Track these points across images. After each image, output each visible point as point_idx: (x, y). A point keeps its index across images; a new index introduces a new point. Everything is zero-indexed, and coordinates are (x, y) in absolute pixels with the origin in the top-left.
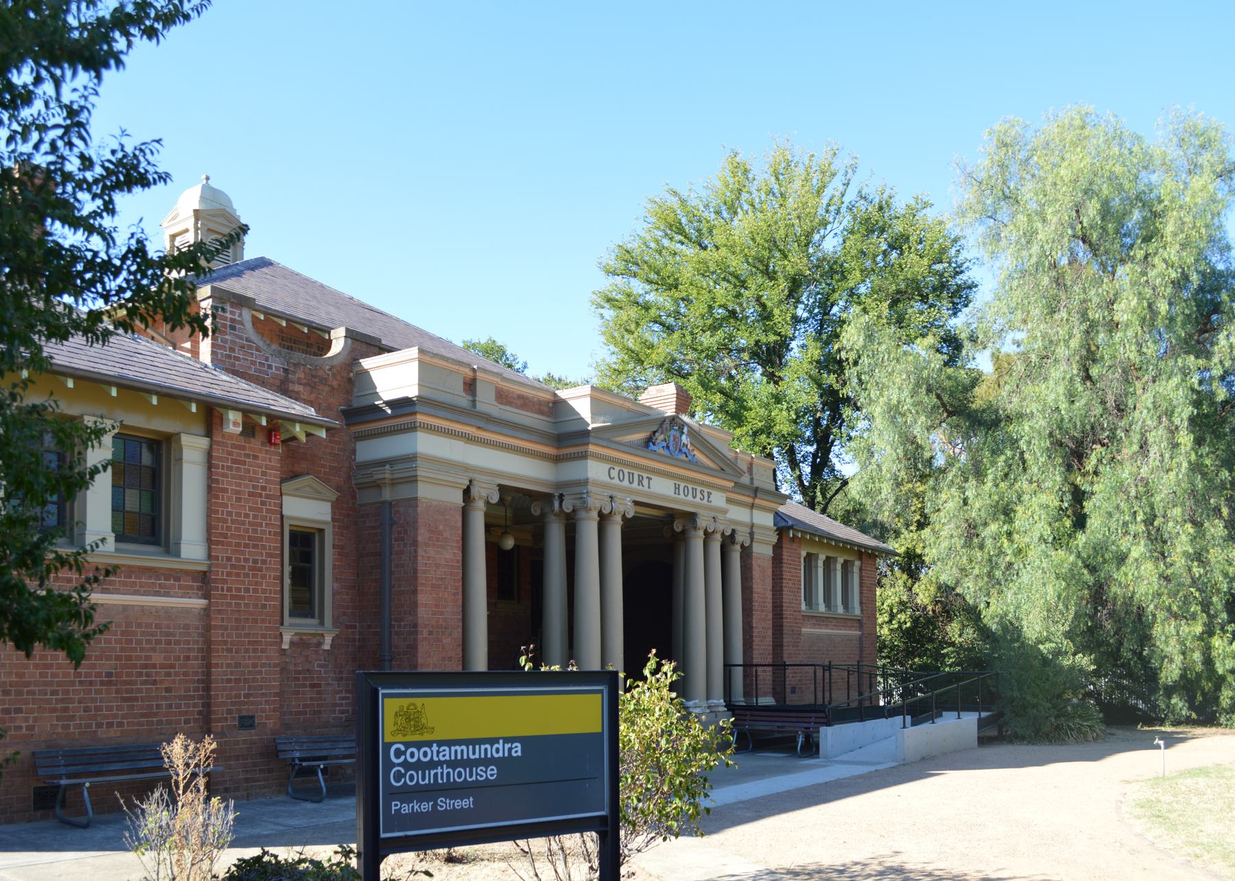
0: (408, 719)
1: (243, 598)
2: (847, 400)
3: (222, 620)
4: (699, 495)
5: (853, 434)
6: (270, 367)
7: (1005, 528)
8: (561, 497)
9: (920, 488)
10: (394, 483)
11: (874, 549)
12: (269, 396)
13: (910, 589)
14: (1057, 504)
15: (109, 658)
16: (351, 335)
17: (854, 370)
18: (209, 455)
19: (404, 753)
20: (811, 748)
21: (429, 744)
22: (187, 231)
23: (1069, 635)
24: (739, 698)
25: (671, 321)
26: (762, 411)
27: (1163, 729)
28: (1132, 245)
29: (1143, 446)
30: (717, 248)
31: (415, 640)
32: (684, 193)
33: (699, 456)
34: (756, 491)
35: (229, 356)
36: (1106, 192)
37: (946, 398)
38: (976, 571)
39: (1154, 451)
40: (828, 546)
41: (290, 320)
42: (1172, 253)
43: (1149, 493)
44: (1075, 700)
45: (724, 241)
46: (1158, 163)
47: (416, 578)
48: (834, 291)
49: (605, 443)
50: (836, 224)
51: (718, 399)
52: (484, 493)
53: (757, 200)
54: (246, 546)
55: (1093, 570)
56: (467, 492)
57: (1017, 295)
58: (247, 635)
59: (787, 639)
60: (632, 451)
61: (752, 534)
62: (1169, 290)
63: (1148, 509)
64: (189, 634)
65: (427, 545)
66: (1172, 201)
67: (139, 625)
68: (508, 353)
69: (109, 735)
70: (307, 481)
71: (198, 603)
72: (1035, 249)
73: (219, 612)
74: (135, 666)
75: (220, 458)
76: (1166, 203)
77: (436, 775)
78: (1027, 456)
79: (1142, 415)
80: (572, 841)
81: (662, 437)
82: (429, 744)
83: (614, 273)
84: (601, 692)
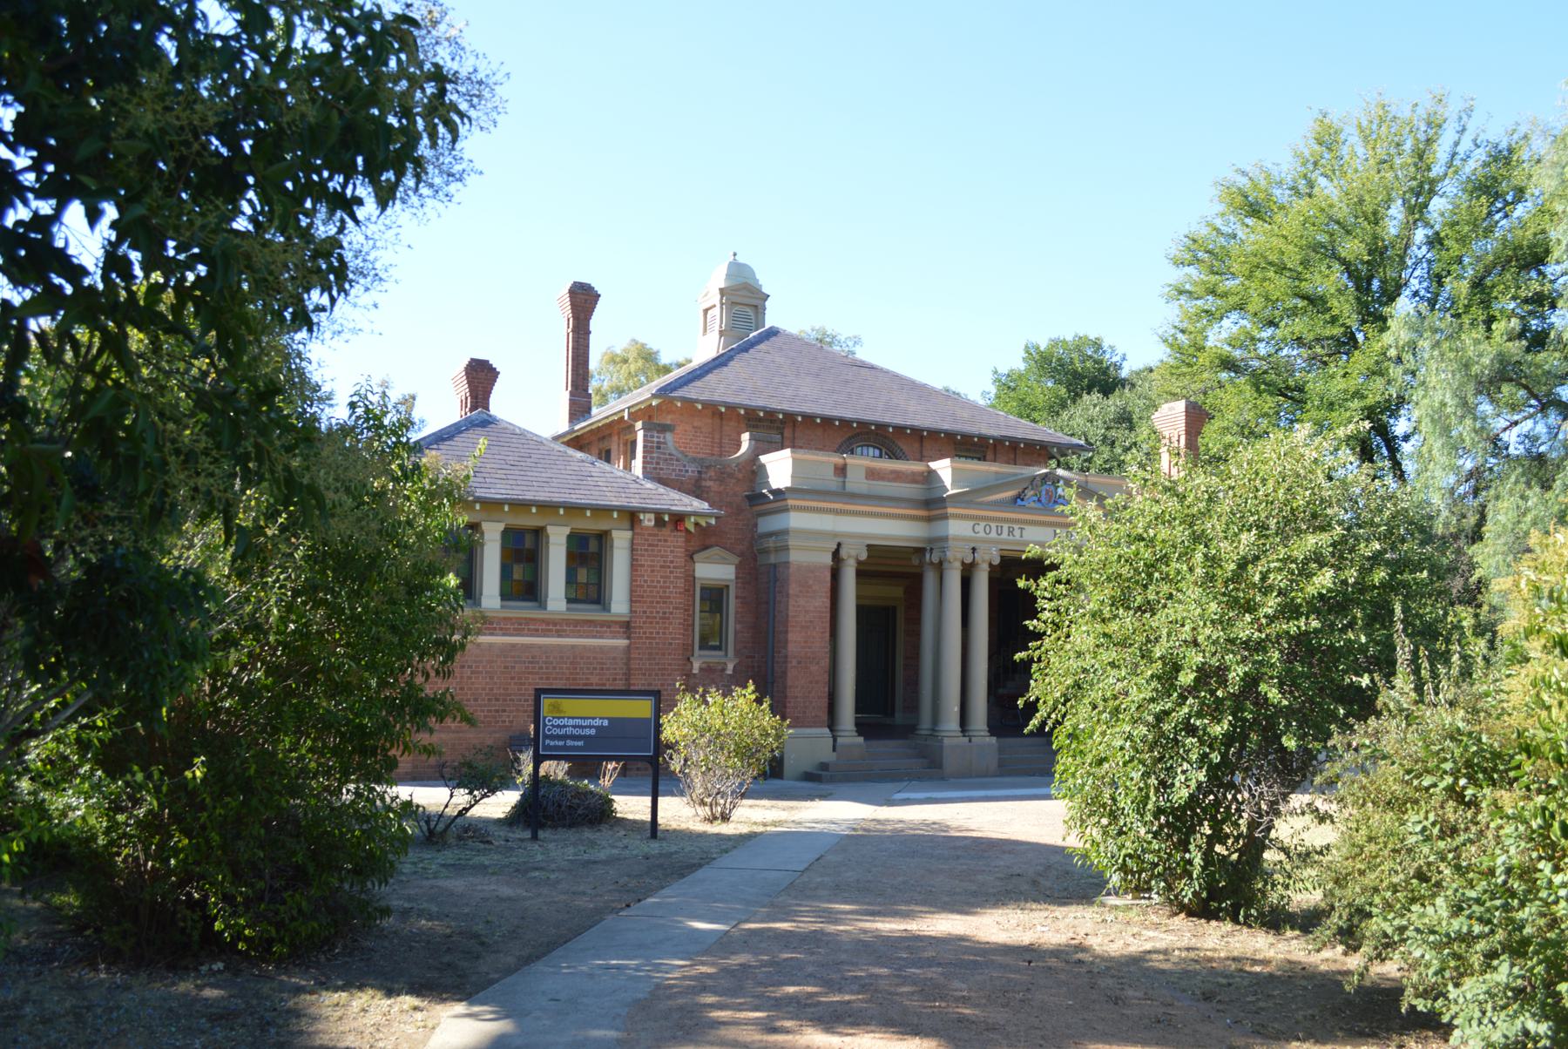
10: (777, 550)
52: (853, 553)
56: (836, 554)
70: (715, 550)
71: (622, 643)
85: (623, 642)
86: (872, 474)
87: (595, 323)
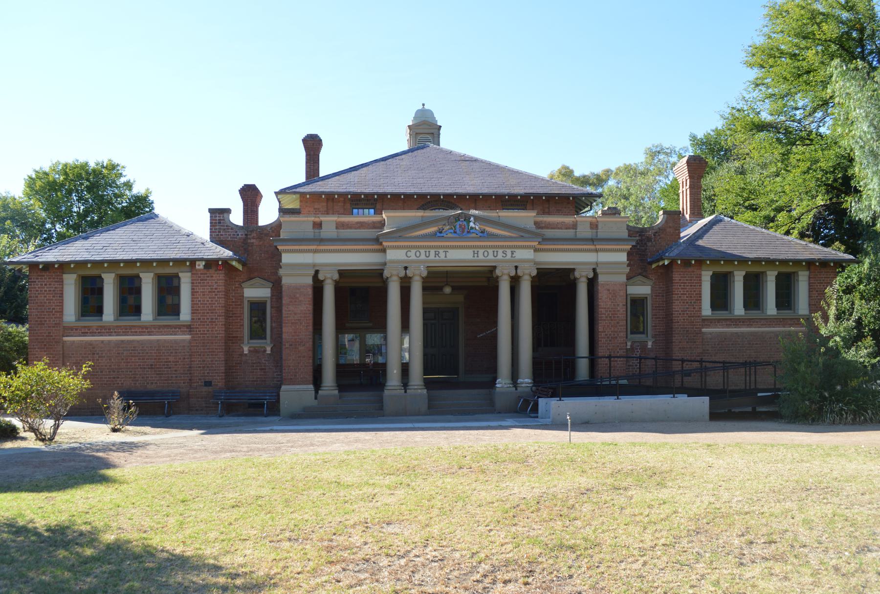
69: (151, 387)
85: (188, 337)
86: (340, 226)
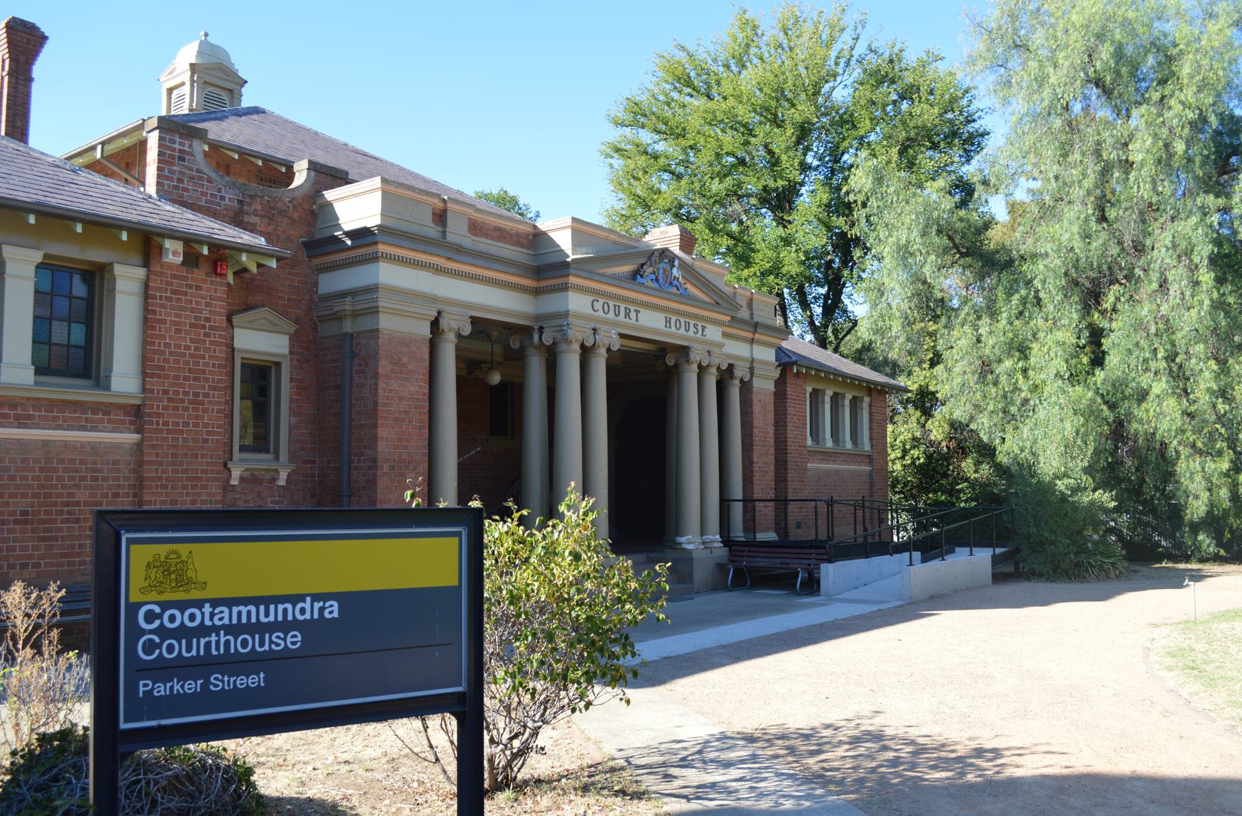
0: (167, 572)
1: (181, 432)
2: (857, 241)
3: (157, 455)
4: (692, 329)
5: (864, 275)
6: (223, 198)
7: (1020, 364)
8: (541, 330)
9: (932, 327)
10: (355, 315)
11: (884, 385)
12: (216, 226)
13: (923, 426)
14: (1074, 341)
15: (24, 496)
16: (314, 166)
17: (863, 212)
18: (146, 286)
19: (160, 616)
20: (812, 586)
21: (199, 604)
22: (183, 84)
23: (1088, 470)
24: (738, 533)
25: (681, 169)
26: (770, 253)
27: (1189, 566)
28: (1148, 88)
29: (1163, 284)
30: (725, 98)
31: (375, 475)
32: (692, 48)
33: (692, 289)
34: (756, 326)
35: (177, 188)
36: (1118, 37)
37: (957, 239)
38: (991, 407)
39: (1174, 289)
40: (835, 381)
41: (267, 160)
42: (1189, 94)
43: (1170, 329)
44: (1096, 537)
45: (731, 91)
46: (1171, 12)
47: (376, 411)
48: (844, 139)
49: (587, 275)
50: (846, 76)
51: (725, 242)
52: (455, 325)
53: (767, 55)
54: (186, 378)
55: (1112, 406)
56: (435, 324)
57: (1030, 139)
58: (184, 471)
59: (791, 474)
60: (617, 283)
61: (752, 369)
62: (1187, 131)
63: (1168, 347)
64: (119, 471)
65: (388, 377)
66: (1187, 45)
67: (61, 461)
68: (521, 203)
70: (263, 312)
71: (130, 438)
72: (1047, 93)
73: (153, 446)
74: (55, 504)
75: (157, 289)
76: (1181, 47)
77: (208, 644)
78: (1042, 295)
79: (1161, 255)
80: (434, 721)
81: (650, 269)
82: (199, 604)
83: (623, 125)
84: (458, 534)
87: (40, 69)
